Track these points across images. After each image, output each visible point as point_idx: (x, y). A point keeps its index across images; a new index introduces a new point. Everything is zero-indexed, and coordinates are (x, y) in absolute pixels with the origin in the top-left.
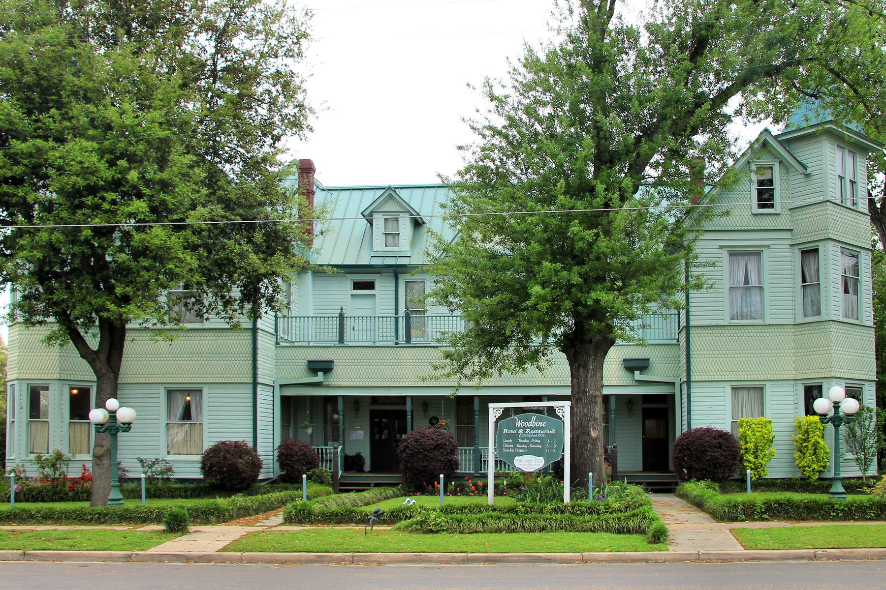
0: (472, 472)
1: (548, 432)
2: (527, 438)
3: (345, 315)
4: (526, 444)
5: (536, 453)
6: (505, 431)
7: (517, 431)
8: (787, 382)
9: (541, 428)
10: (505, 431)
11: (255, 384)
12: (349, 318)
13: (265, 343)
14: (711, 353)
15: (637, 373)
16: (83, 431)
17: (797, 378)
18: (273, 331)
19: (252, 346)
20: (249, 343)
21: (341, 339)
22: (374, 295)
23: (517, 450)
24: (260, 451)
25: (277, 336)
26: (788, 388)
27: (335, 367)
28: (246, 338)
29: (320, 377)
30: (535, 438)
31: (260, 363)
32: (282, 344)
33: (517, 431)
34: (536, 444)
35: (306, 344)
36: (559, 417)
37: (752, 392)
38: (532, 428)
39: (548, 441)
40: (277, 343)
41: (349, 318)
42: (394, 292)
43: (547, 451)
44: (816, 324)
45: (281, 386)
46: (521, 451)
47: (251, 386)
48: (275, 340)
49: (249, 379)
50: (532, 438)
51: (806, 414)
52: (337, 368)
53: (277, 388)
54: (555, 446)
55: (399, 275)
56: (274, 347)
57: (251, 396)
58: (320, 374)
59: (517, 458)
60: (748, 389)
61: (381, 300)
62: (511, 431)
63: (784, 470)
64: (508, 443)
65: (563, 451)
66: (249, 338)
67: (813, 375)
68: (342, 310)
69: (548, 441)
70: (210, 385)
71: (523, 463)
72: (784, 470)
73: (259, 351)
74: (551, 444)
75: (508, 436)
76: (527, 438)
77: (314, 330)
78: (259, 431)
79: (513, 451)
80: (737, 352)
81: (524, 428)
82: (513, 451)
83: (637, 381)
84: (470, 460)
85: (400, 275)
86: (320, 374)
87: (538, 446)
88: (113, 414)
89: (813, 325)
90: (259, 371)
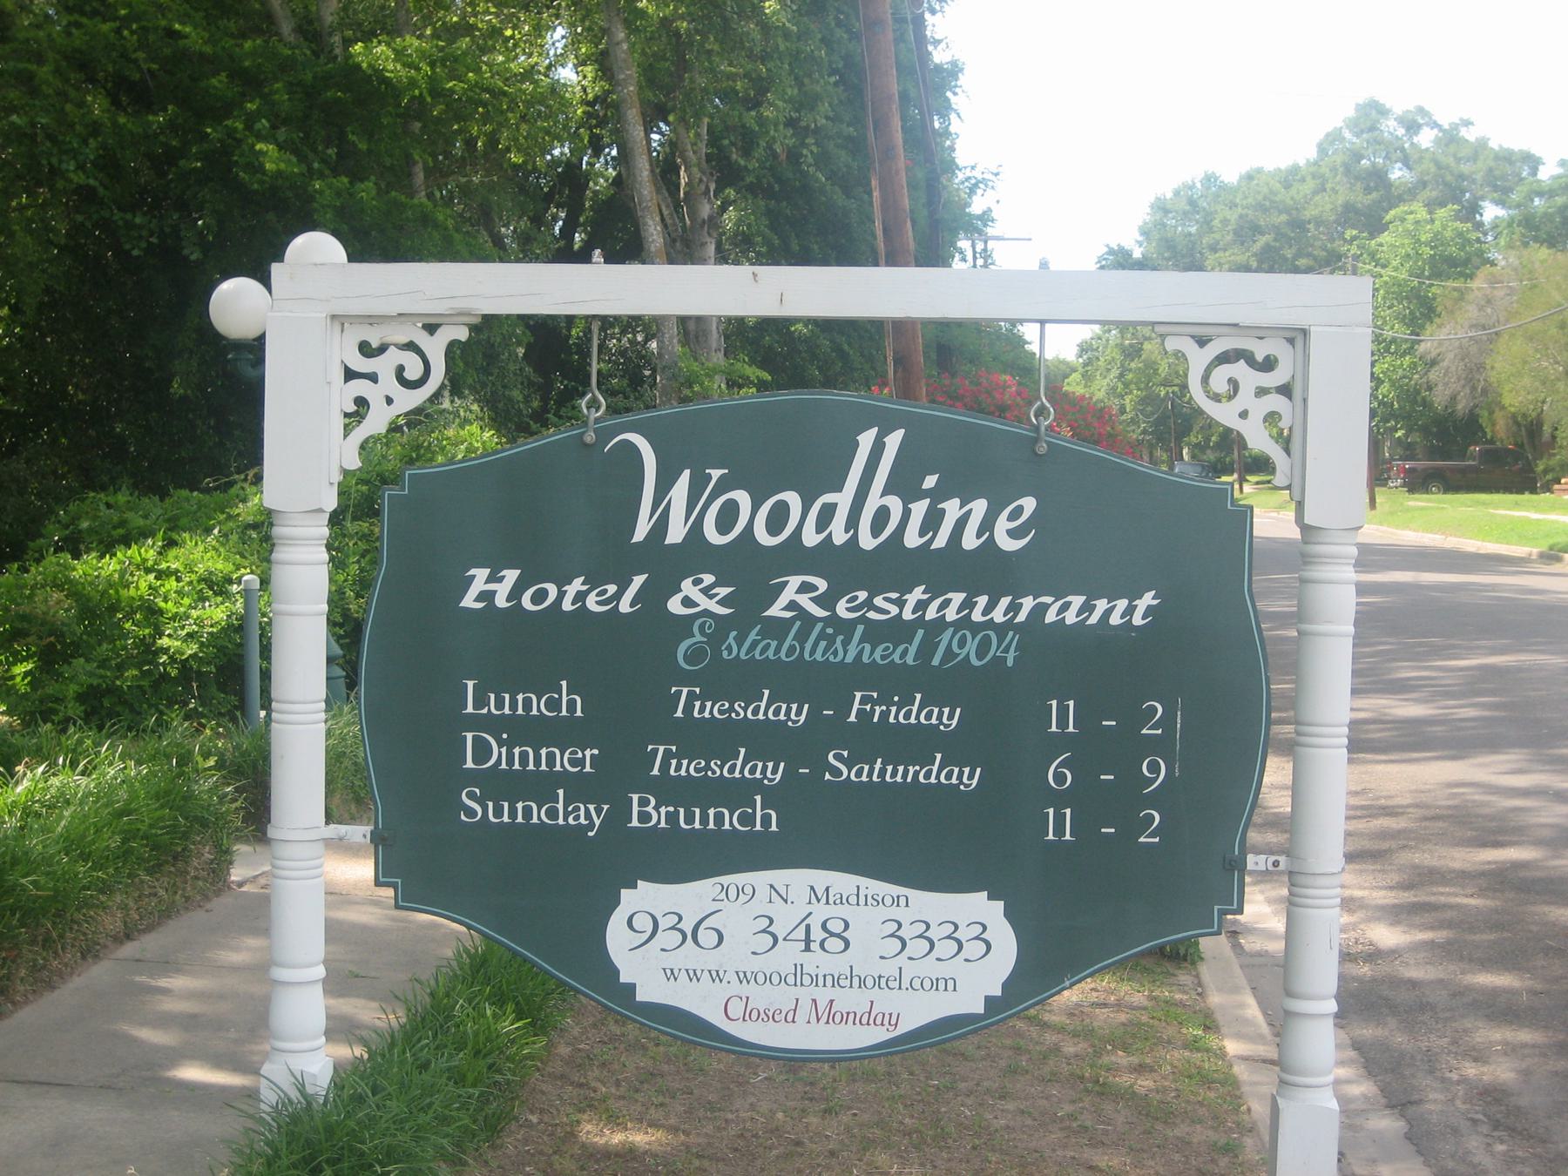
1: (1069, 610)
4: (764, 741)
7: (654, 597)
16: (1382, 893)
18: (678, 926)
33: (654, 597)
34: (914, 746)
43: (1059, 825)
46: (694, 821)
50: (861, 675)
51: (327, 823)
63: (1309, 901)
69: (1062, 717)
71: (735, 956)
79: (589, 816)
82: (589, 816)
87: (935, 773)
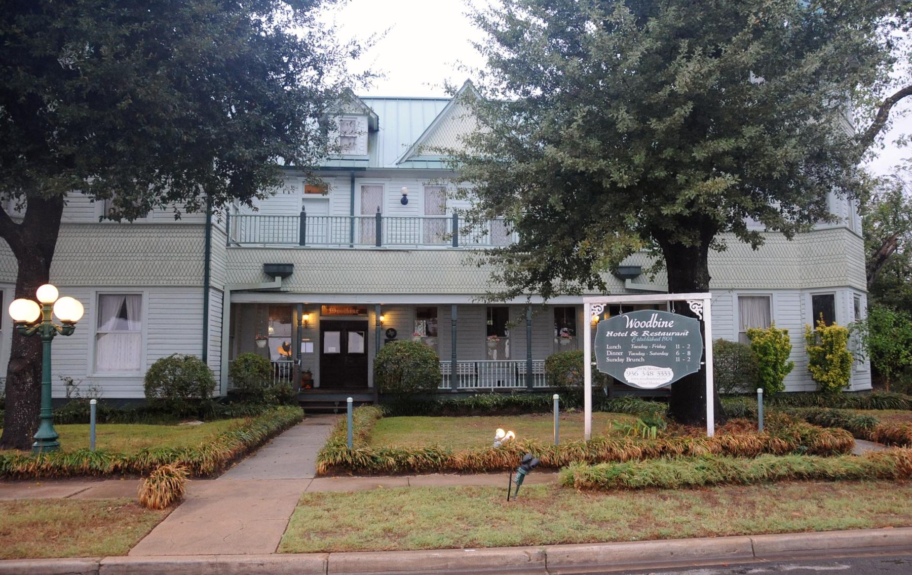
0: (448, 388)
2: (645, 343)
3: (307, 215)
4: (642, 350)
5: (660, 362)
6: (609, 334)
7: (629, 334)
8: (794, 292)
9: (668, 330)
10: (609, 334)
11: (207, 287)
12: (311, 219)
13: (217, 240)
14: (717, 259)
15: (628, 281)
17: (804, 287)
19: (204, 244)
20: (202, 240)
21: (302, 242)
22: (328, 200)
23: (629, 360)
24: (213, 362)
25: (228, 236)
26: (794, 297)
27: (294, 271)
28: (197, 235)
29: (278, 282)
30: (657, 343)
31: (213, 264)
32: (232, 246)
34: (660, 350)
35: (262, 246)
36: (693, 315)
37: (757, 302)
38: (651, 330)
39: (678, 346)
40: (228, 244)
41: (311, 219)
42: (349, 197)
43: (678, 359)
44: (825, 232)
45: (232, 292)
46: (634, 360)
47: (202, 290)
48: (226, 241)
49: (199, 282)
50: (654, 342)
52: (298, 274)
53: (227, 294)
54: (689, 353)
55: (356, 179)
56: (224, 248)
57: (202, 302)
58: (278, 279)
59: (628, 370)
60: (753, 298)
61: (335, 205)
62: (619, 334)
64: (614, 350)
65: (703, 359)
66: (201, 235)
67: (823, 285)
68: (303, 209)
69: (678, 346)
70: (151, 289)
72: (795, 383)
73: (213, 250)
74: (683, 350)
75: (614, 341)
76: (645, 343)
77: (262, 231)
78: (209, 343)
79: (622, 360)
80: (744, 259)
81: (640, 331)
82: (622, 360)
83: (627, 290)
84: (494, 374)
85: (356, 179)
86: (278, 279)
87: (663, 354)
88: (47, 308)
89: (822, 232)
90: (212, 273)
